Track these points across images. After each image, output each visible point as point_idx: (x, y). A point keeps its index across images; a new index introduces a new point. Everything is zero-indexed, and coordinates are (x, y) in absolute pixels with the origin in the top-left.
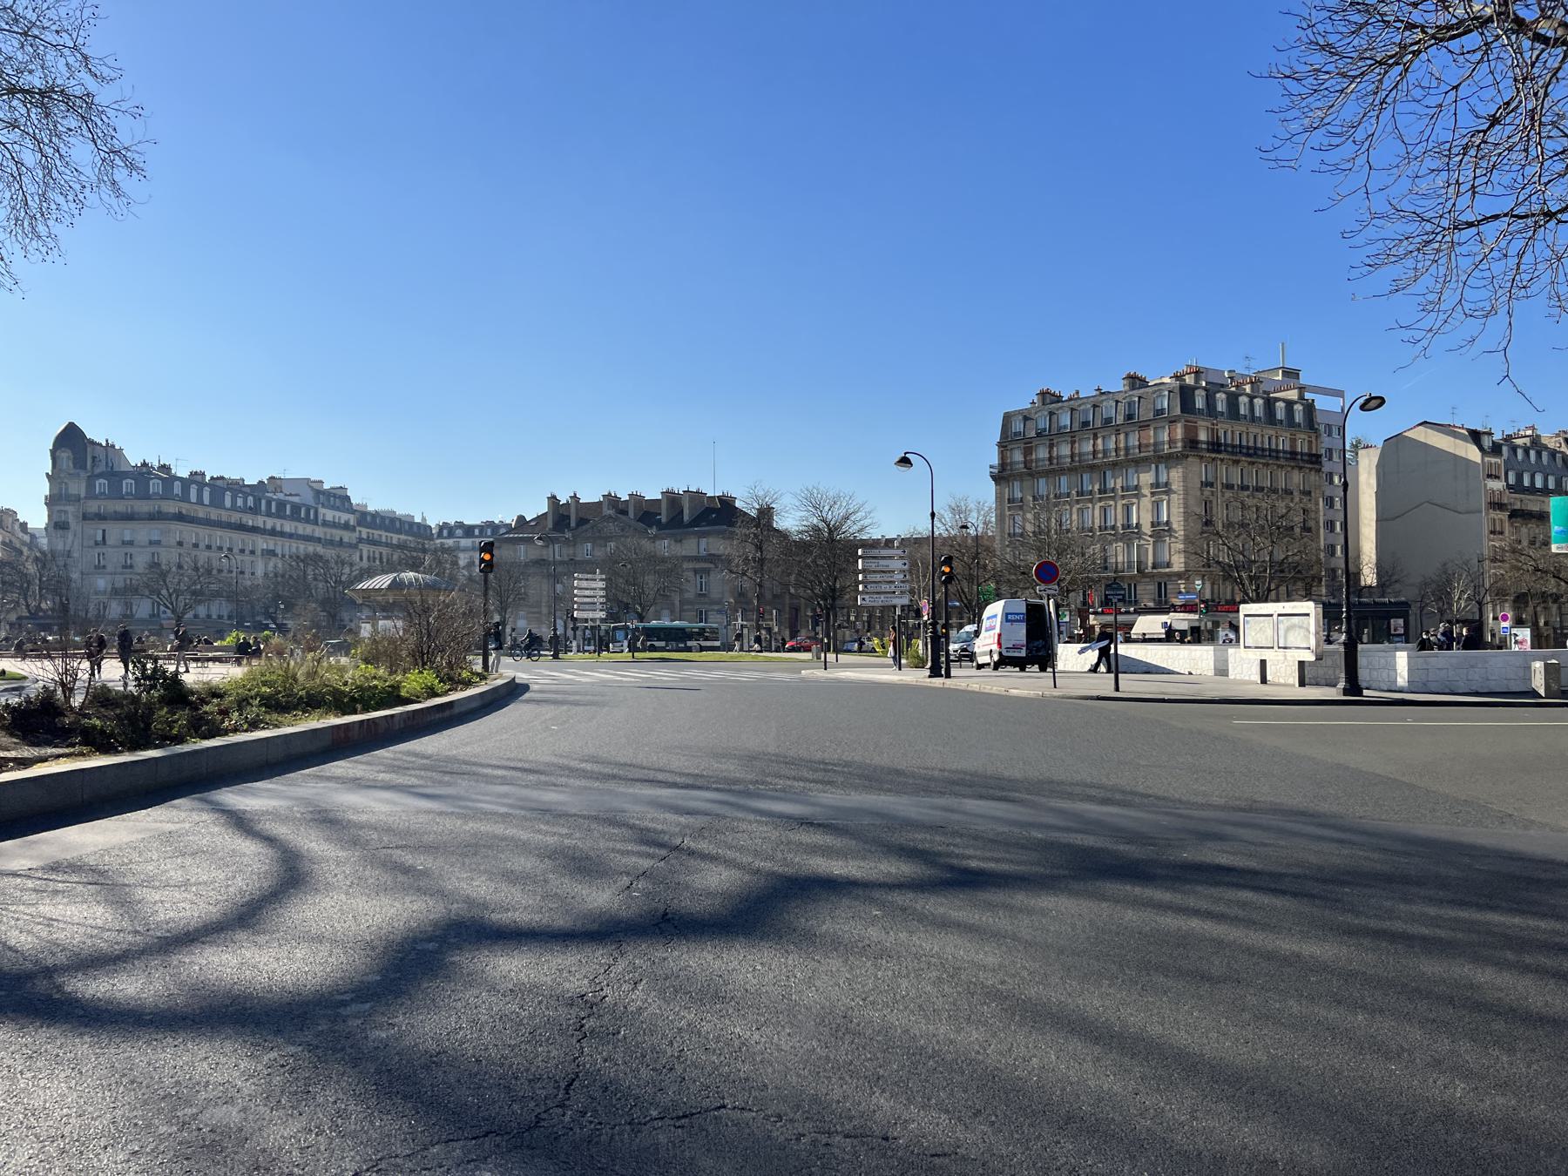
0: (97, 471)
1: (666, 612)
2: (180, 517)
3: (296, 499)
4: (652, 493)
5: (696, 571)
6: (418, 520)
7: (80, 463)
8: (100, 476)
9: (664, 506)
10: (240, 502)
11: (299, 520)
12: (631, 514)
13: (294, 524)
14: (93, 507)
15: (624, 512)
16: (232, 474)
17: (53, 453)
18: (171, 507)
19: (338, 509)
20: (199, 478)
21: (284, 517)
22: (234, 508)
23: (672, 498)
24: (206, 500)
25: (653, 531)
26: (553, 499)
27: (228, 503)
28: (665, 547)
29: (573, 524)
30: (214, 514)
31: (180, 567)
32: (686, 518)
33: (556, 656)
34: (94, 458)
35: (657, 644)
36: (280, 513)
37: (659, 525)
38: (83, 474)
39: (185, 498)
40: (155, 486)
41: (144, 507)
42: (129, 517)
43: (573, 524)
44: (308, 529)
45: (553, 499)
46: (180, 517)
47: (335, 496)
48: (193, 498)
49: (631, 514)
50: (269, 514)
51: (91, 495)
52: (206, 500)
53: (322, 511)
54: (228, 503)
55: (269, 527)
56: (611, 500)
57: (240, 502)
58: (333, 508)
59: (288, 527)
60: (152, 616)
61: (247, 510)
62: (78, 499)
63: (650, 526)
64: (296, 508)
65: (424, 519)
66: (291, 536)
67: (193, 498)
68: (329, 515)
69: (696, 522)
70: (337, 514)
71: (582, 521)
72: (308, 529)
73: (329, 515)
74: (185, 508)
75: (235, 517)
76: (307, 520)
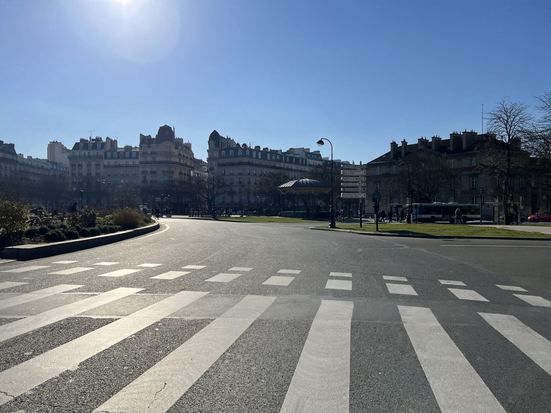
0: (224, 148)
1: (452, 198)
2: (249, 164)
3: (298, 156)
4: (445, 136)
5: (469, 176)
6: (351, 163)
7: (217, 145)
8: (224, 150)
9: (451, 143)
10: (274, 158)
11: (298, 164)
12: (433, 148)
13: (296, 166)
14: (221, 161)
15: (430, 147)
16: (272, 147)
17: (209, 142)
18: (245, 160)
19: (315, 159)
20: (266, 150)
21: (292, 163)
22: (271, 160)
23: (455, 136)
24: (260, 157)
25: (444, 155)
26: (394, 145)
27: (269, 158)
28: (453, 163)
29: (403, 155)
30: (263, 162)
31: (249, 183)
32: (464, 146)
33: (333, 226)
34: (222, 143)
35: (436, 216)
36: (291, 162)
37: (449, 152)
38: (218, 149)
39: (251, 156)
40: (240, 152)
41: (237, 160)
42: (231, 164)
43: (403, 155)
44: (303, 168)
45: (394, 145)
46: (249, 164)
47: (314, 154)
48: (254, 156)
49: (433, 148)
50: (286, 162)
51: (220, 157)
52: (260, 157)
53: (308, 160)
54: (269, 158)
55: (286, 167)
56: (422, 141)
57: (274, 158)
58: (313, 159)
59: (294, 167)
60: (239, 202)
61: (277, 160)
62: (216, 158)
63: (443, 153)
64: (297, 159)
65: (353, 163)
66: (295, 170)
67: (254, 156)
68: (312, 162)
69: (470, 148)
70: (315, 161)
71: (407, 154)
72: (303, 168)
73: (312, 162)
74: (251, 160)
75: (272, 163)
76: (302, 164)
